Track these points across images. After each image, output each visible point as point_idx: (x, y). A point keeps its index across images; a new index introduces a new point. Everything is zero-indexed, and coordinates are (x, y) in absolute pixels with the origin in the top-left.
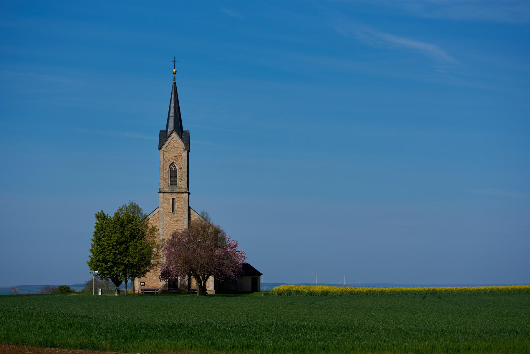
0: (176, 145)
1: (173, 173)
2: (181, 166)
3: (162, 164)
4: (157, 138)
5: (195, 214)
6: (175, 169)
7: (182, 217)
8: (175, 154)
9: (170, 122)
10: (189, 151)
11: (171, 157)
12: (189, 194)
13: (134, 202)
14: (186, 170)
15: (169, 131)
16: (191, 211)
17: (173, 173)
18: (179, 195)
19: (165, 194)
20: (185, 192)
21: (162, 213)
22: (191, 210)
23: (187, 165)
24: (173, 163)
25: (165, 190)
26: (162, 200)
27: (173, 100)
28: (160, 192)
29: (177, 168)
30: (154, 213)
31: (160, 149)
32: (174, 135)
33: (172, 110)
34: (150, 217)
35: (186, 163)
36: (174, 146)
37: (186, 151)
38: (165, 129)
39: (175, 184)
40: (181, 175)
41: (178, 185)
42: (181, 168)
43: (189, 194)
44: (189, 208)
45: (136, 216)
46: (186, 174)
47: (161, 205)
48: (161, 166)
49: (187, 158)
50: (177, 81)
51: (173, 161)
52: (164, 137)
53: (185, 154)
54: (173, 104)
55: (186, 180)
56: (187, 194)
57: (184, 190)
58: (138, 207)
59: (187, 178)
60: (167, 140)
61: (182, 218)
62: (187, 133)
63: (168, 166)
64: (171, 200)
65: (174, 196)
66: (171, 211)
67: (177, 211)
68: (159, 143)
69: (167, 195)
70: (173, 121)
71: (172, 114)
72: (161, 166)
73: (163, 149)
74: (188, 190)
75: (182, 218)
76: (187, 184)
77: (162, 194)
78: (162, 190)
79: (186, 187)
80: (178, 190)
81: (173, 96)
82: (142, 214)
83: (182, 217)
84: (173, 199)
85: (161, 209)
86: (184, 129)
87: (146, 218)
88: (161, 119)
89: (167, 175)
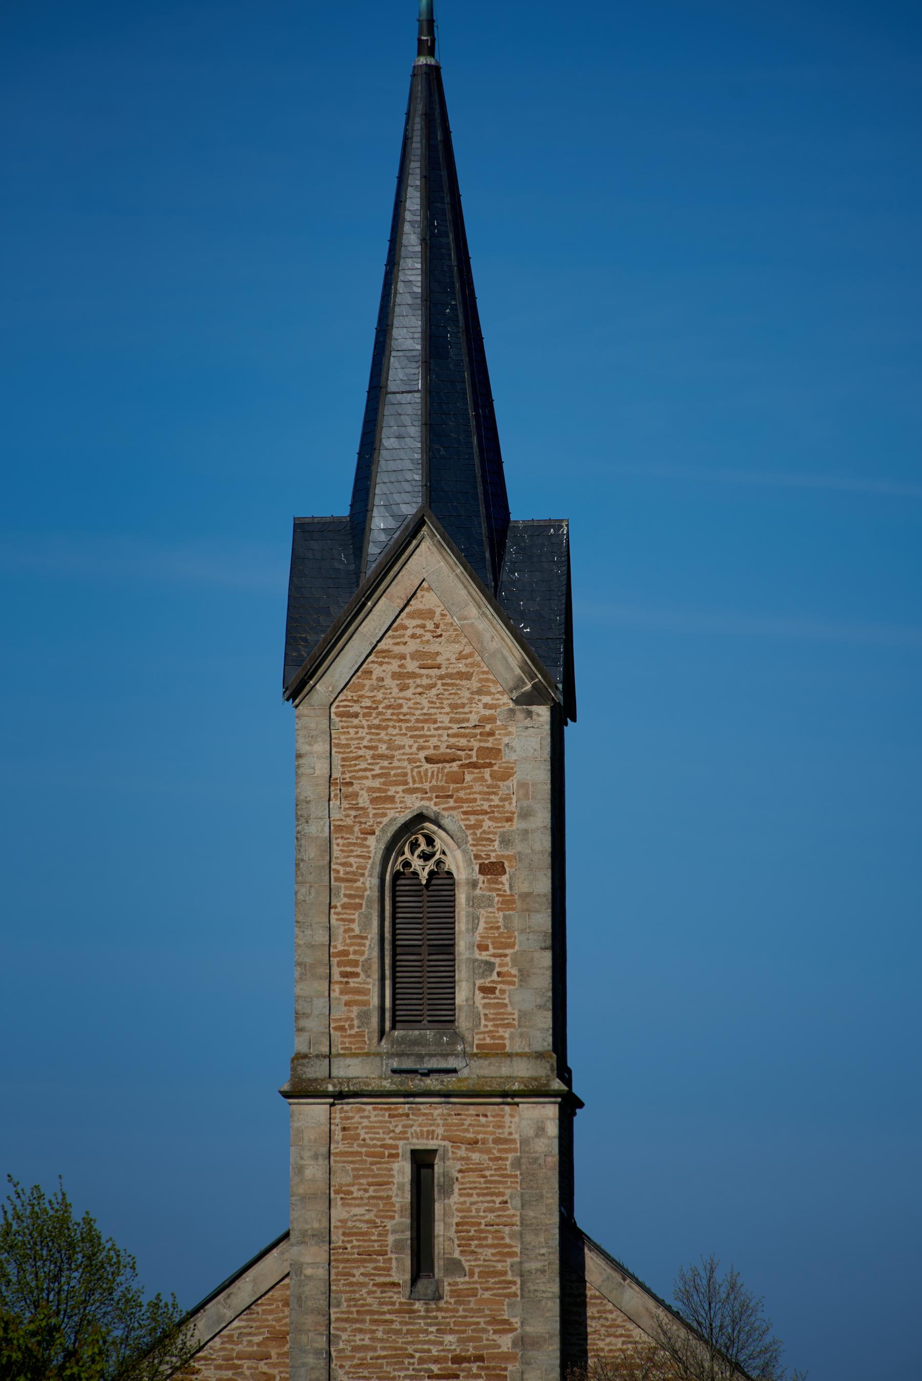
0: (447, 652)
1: (417, 915)
2: (495, 852)
3: (317, 829)
4: (269, 577)
5: (633, 1298)
6: (442, 879)
7: (504, 1327)
8: (441, 743)
9: (388, 441)
10: (564, 712)
11: (401, 763)
12: (569, 1105)
13: (50, 1192)
14: (544, 885)
15: (380, 524)
16: (595, 1270)
17: (417, 915)
18: (477, 1120)
19: (348, 1107)
20: (536, 1092)
21: (313, 1292)
22: (591, 1260)
23: (544, 842)
24: (420, 818)
25: (351, 1070)
26: (314, 1171)
27: (412, 239)
28: (300, 1091)
29: (459, 864)
30: (244, 1291)
31: (297, 689)
32: (431, 561)
33: (408, 334)
34: (201, 1328)
35: (543, 817)
36: (428, 661)
37: (543, 713)
38: (341, 508)
39: (442, 1014)
40: (491, 931)
41: (463, 1023)
42: (492, 869)
43: (569, 1105)
44: (572, 1242)
45: (68, 1326)
46: (543, 920)
47: (307, 1218)
48: (311, 852)
49: (542, 775)
50: (443, 57)
51: (414, 804)
52: (332, 583)
53: (525, 741)
54: (412, 272)
55: (543, 980)
56: (550, 1112)
57: (522, 1071)
58: (92, 1238)
59: (546, 959)
60: (359, 609)
61: (506, 1342)
62: (550, 548)
63: (375, 846)
64: (402, 1171)
65: (428, 1126)
66: (401, 1271)
67: (454, 1266)
68: (289, 661)
69: (366, 1116)
70: (414, 431)
71: (406, 373)
72: (311, 852)
73: (323, 689)
74: (564, 1072)
75: (506, 1342)
76: (545, 1020)
77: (314, 1112)
78: (316, 1070)
79: (544, 1040)
80: (472, 1072)
81: (414, 202)
82: (131, 1301)
83: (504, 1327)
84: (422, 1161)
85: (311, 1256)
86: (522, 508)
87: (168, 1336)
88: (308, 425)
89: (360, 933)
